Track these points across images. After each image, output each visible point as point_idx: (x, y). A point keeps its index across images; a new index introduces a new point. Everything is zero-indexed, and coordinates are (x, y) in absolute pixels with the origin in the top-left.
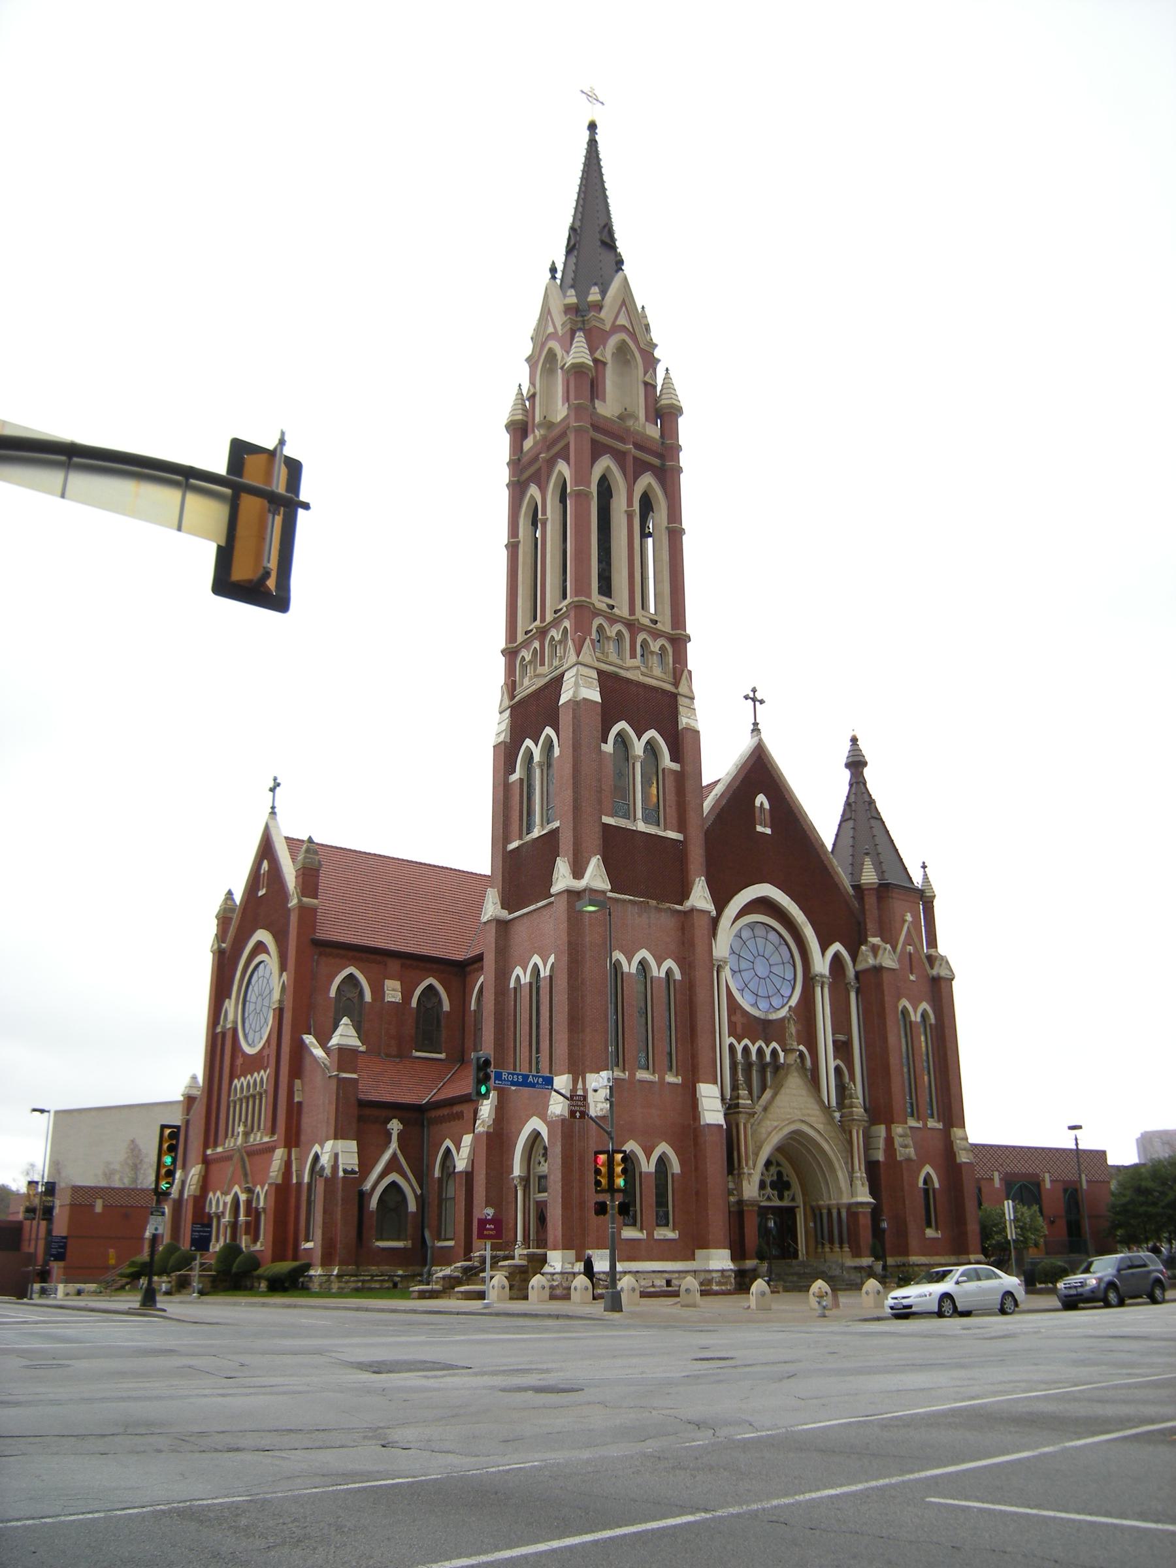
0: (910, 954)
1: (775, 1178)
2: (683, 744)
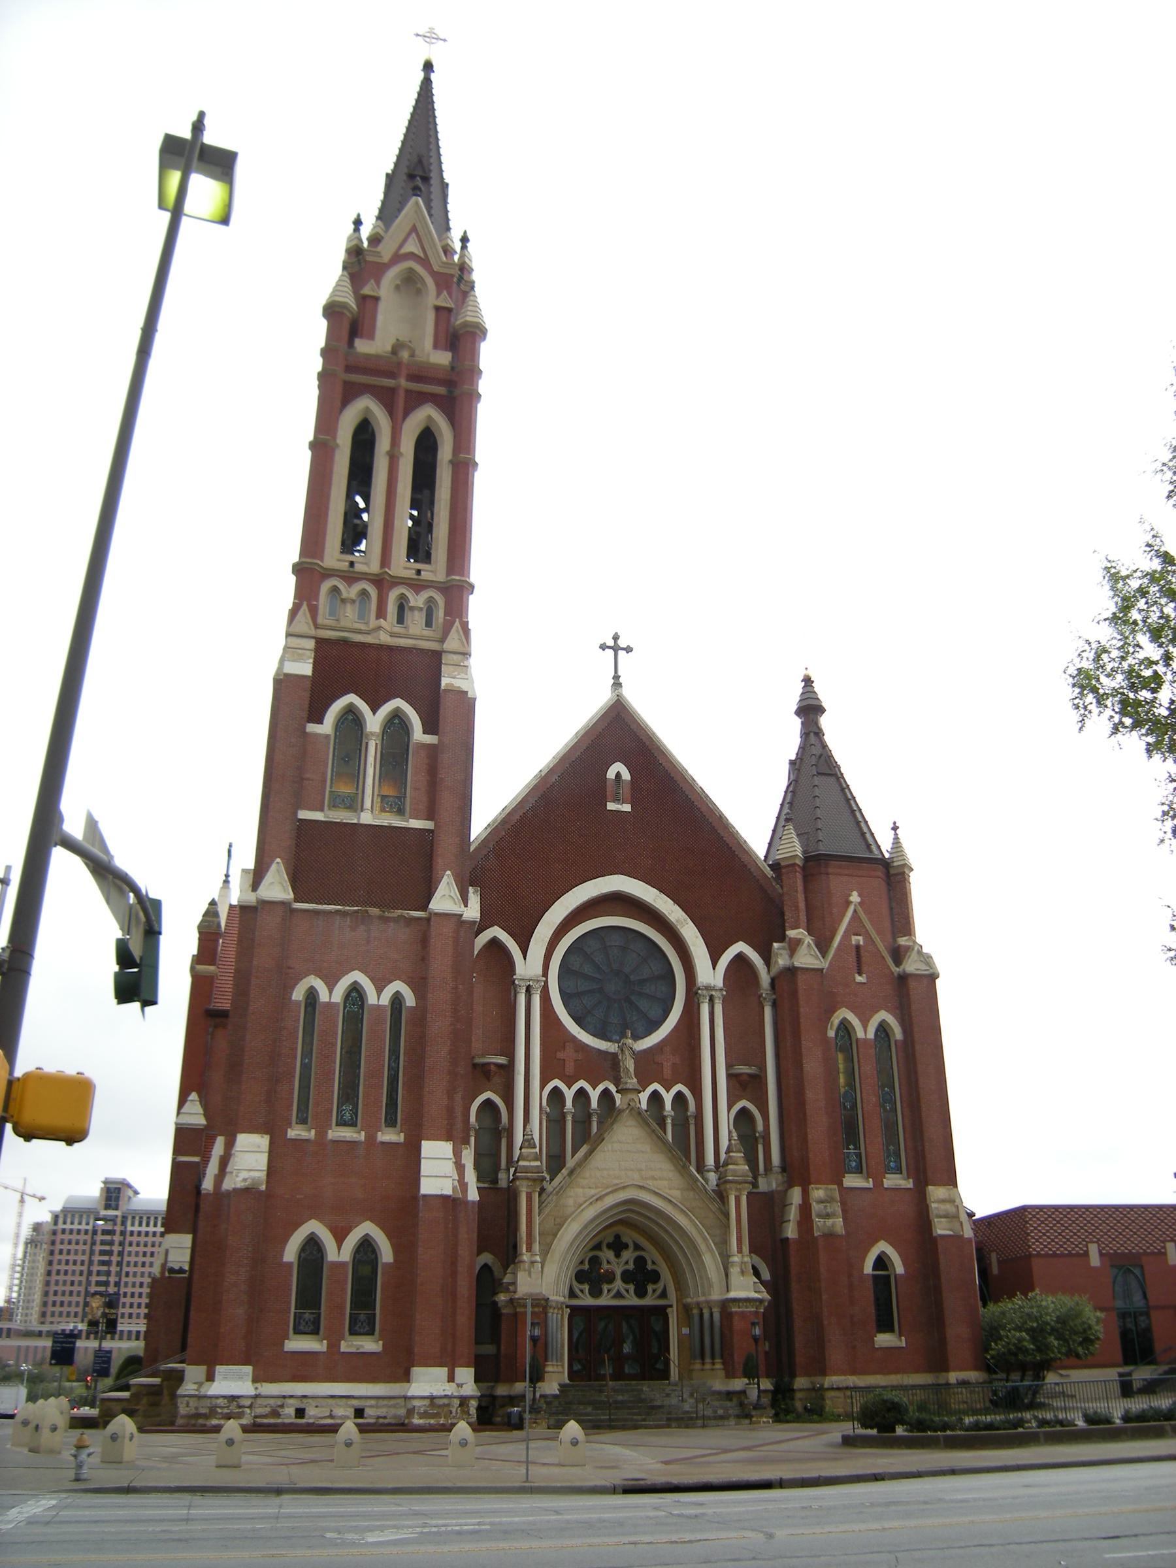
0: (858, 947)
1: (631, 1266)
2: (450, 716)
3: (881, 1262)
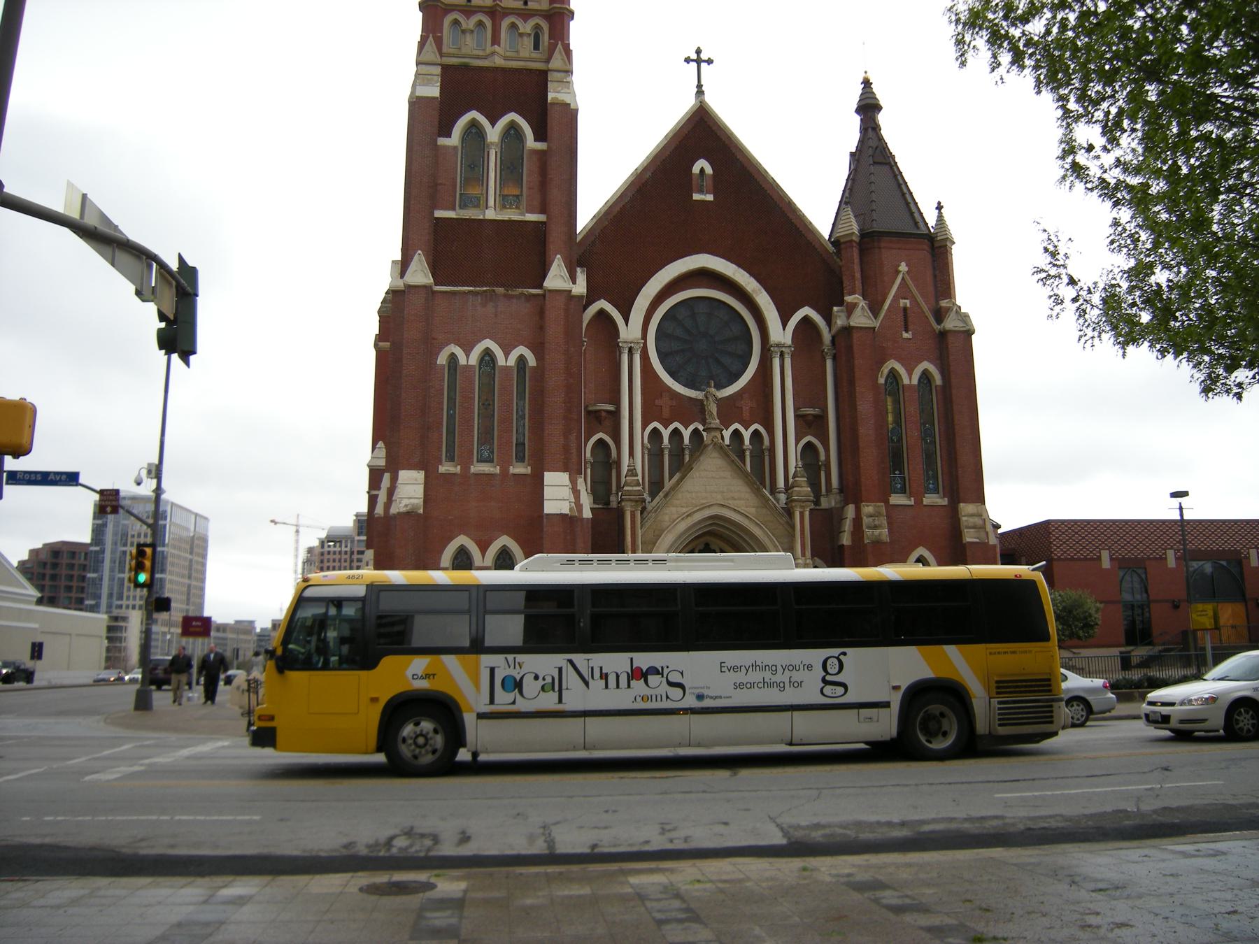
0: (905, 309)
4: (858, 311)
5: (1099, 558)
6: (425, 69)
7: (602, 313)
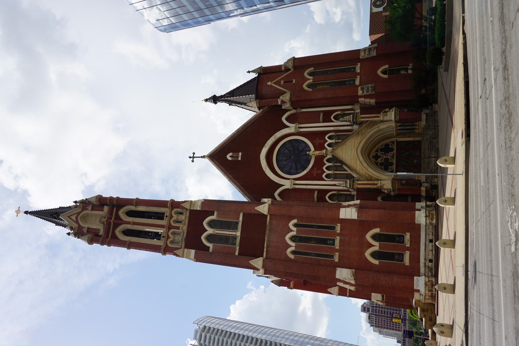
0: (284, 82)
3: (384, 72)
4: (284, 99)
5: (385, 16)
6: (185, 255)
7: (280, 195)
